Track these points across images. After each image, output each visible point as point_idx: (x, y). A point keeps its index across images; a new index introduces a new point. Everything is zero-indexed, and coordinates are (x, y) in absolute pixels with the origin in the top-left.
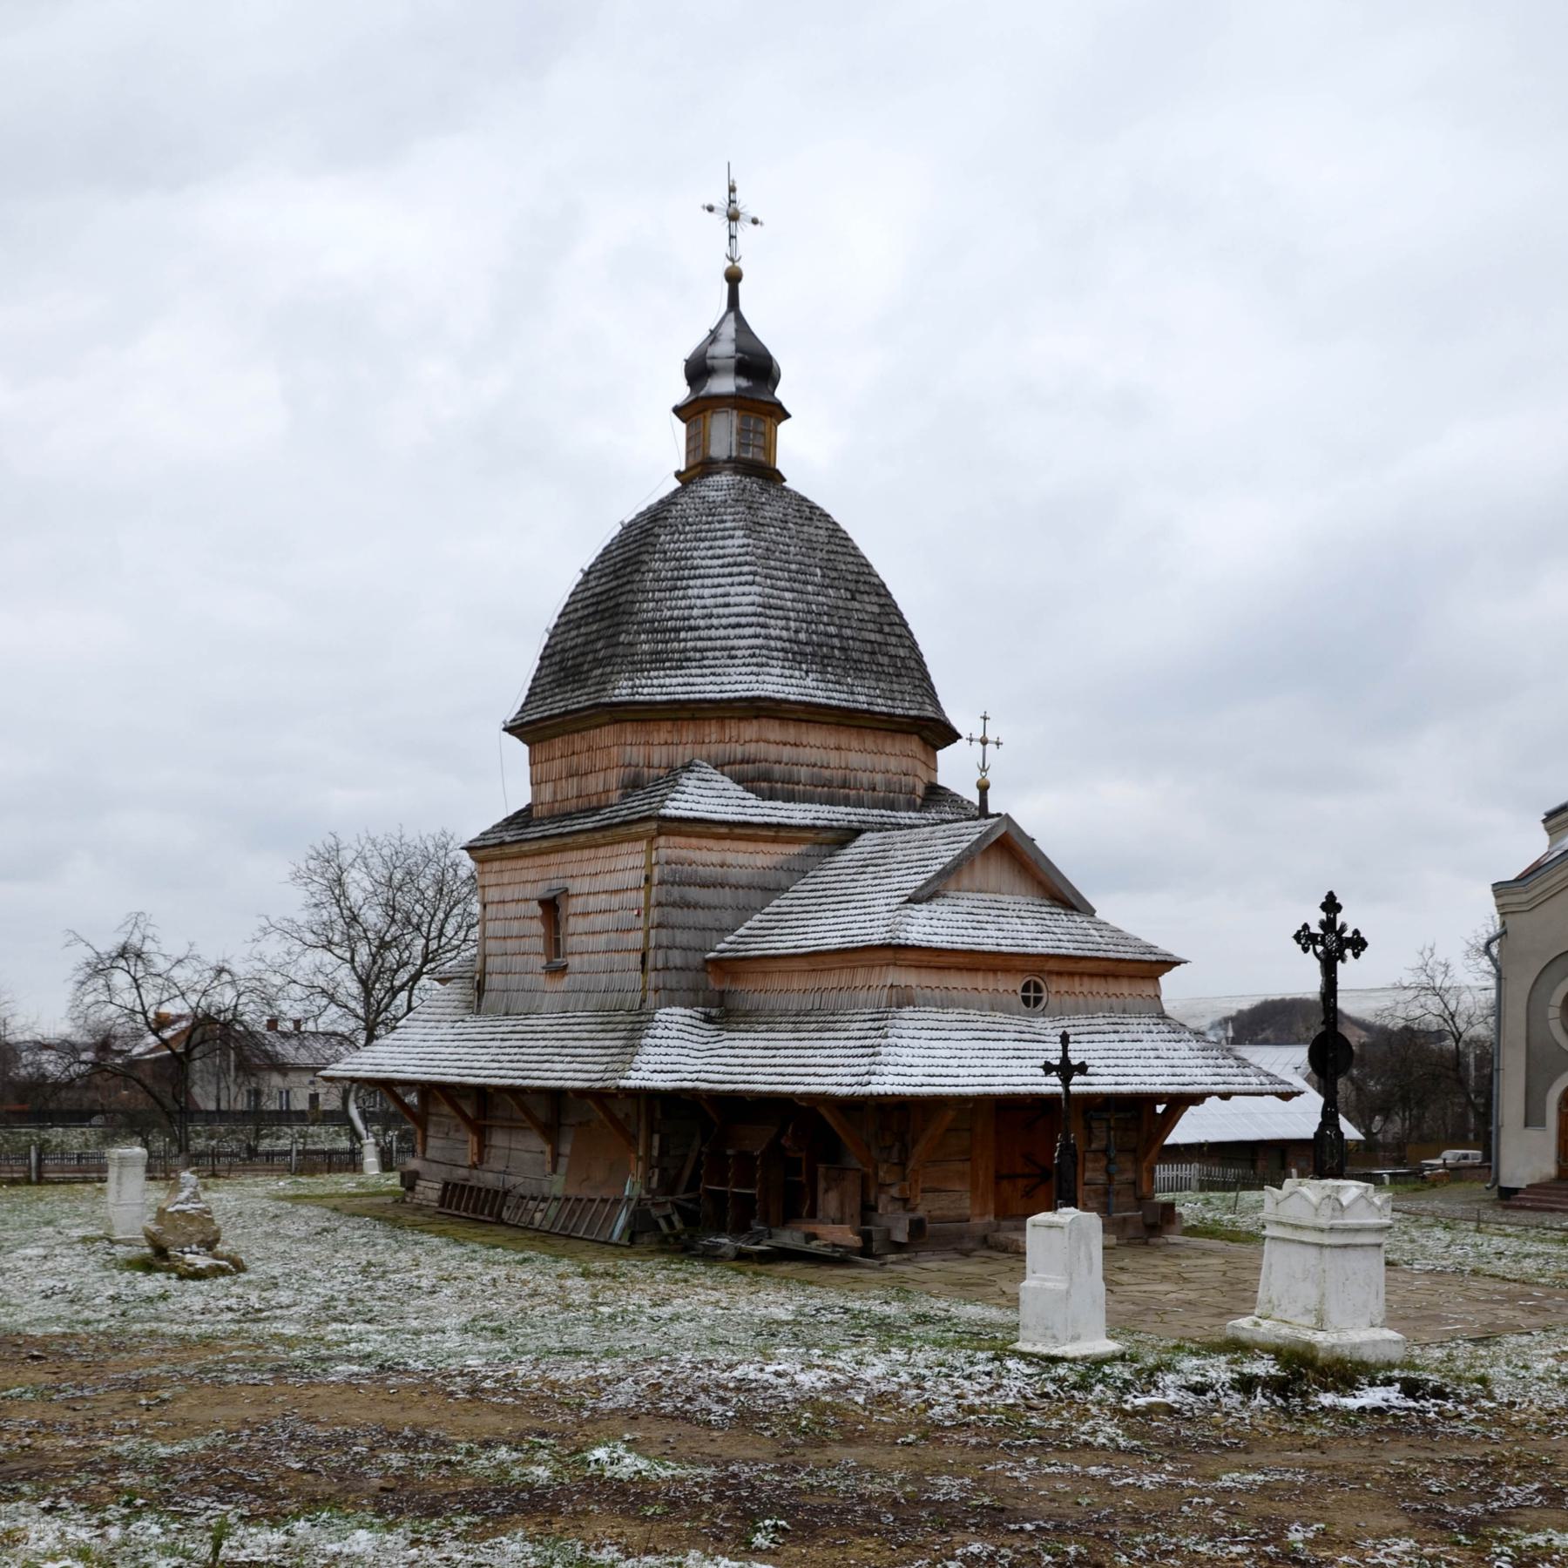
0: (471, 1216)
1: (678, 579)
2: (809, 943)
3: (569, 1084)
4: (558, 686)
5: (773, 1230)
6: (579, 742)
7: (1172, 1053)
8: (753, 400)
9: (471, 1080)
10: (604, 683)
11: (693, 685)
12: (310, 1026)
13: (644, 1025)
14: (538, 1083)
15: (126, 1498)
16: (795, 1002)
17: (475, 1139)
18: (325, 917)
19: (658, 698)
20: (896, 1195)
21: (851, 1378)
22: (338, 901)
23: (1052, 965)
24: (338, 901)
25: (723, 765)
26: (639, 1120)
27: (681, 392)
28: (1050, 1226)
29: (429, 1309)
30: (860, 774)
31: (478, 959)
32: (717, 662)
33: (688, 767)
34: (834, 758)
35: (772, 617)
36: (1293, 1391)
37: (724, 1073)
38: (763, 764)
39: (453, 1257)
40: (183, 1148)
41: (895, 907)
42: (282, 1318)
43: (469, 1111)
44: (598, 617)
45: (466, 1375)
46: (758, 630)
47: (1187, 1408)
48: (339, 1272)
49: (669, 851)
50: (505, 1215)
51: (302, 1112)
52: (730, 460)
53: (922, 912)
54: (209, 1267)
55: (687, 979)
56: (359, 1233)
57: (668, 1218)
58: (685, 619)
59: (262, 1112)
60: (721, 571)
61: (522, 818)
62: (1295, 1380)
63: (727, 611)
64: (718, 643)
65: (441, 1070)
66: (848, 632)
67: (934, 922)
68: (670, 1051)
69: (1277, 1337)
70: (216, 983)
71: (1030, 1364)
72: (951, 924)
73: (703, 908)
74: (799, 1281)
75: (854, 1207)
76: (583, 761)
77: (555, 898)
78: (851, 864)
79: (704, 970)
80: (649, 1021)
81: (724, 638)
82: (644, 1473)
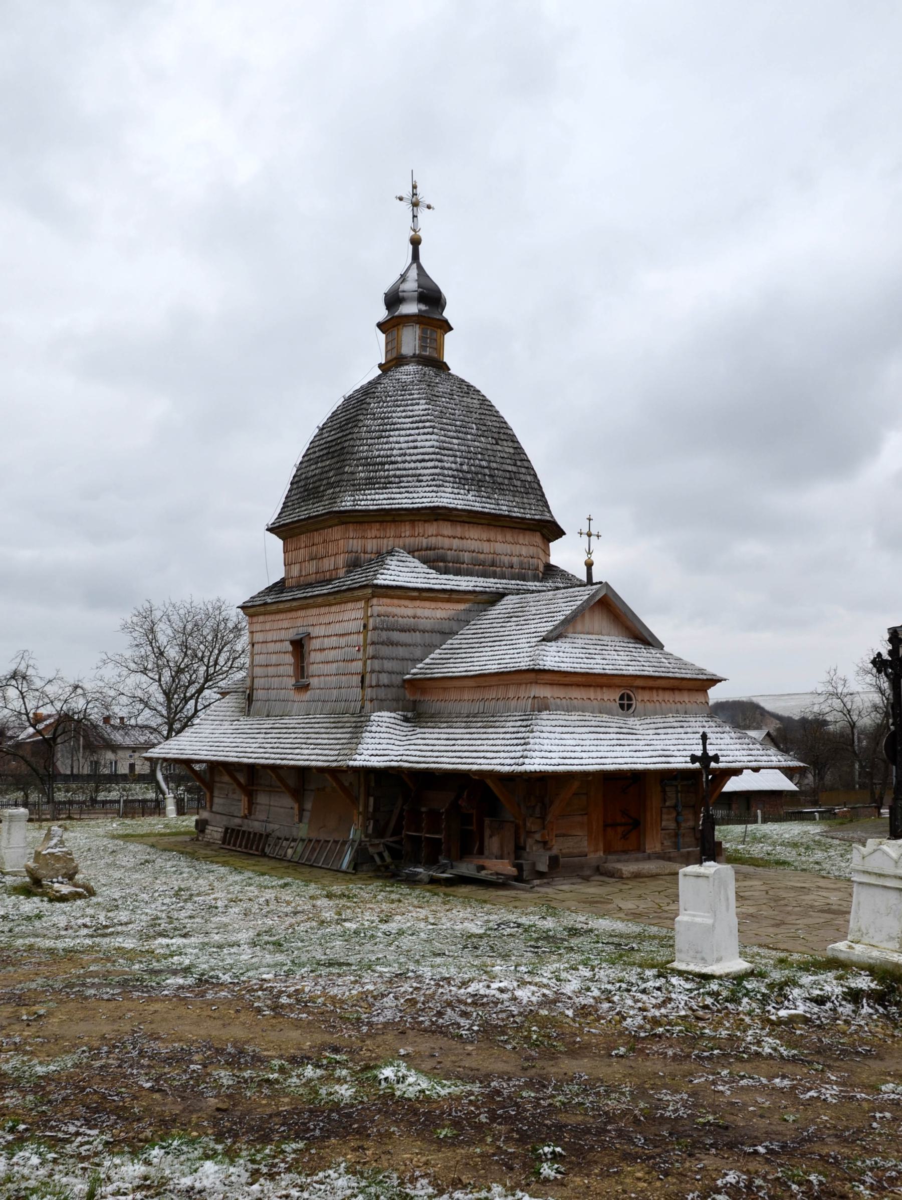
0: (244, 850)
1: (383, 431)
2: (476, 668)
3: (314, 764)
4: (303, 501)
5: (454, 863)
6: (317, 537)
7: (719, 741)
8: (429, 318)
9: (246, 760)
10: (335, 498)
11: (394, 499)
12: (133, 722)
13: (364, 724)
14: (292, 763)
15: (11, 1124)
16: (465, 708)
17: (246, 799)
18: (143, 653)
19: (371, 507)
20: (539, 839)
21: (555, 992)
22: (151, 643)
23: (639, 683)
24: (151, 643)
25: (414, 552)
26: (359, 787)
27: (382, 314)
28: (698, 876)
29: (226, 925)
30: (503, 557)
31: (248, 679)
32: (410, 484)
33: (391, 553)
34: (486, 547)
35: (445, 455)
36: (889, 1001)
37: (419, 756)
39: (236, 882)
40: (50, 801)
41: (534, 644)
42: (122, 933)
43: (242, 780)
44: (330, 456)
45: (265, 990)
46: (437, 463)
47: (815, 1016)
48: (160, 896)
49: (380, 608)
50: (267, 850)
51: (125, 775)
52: (414, 356)
53: (552, 647)
54: (70, 893)
55: (391, 693)
56: (169, 864)
57: (380, 855)
58: (388, 457)
59: (100, 776)
60: (411, 426)
61: (279, 587)
62: (889, 992)
63: (415, 451)
64: (410, 472)
65: (225, 753)
66: (494, 465)
67: (561, 654)
68: (381, 741)
69: (870, 958)
70: (73, 695)
71: (687, 980)
72: (572, 655)
73: (402, 646)
74: (476, 900)
75: (510, 847)
76: (320, 550)
77: (301, 639)
78: (500, 616)
79: (403, 687)
80: (367, 721)
81: (414, 469)
82: (427, 1093)
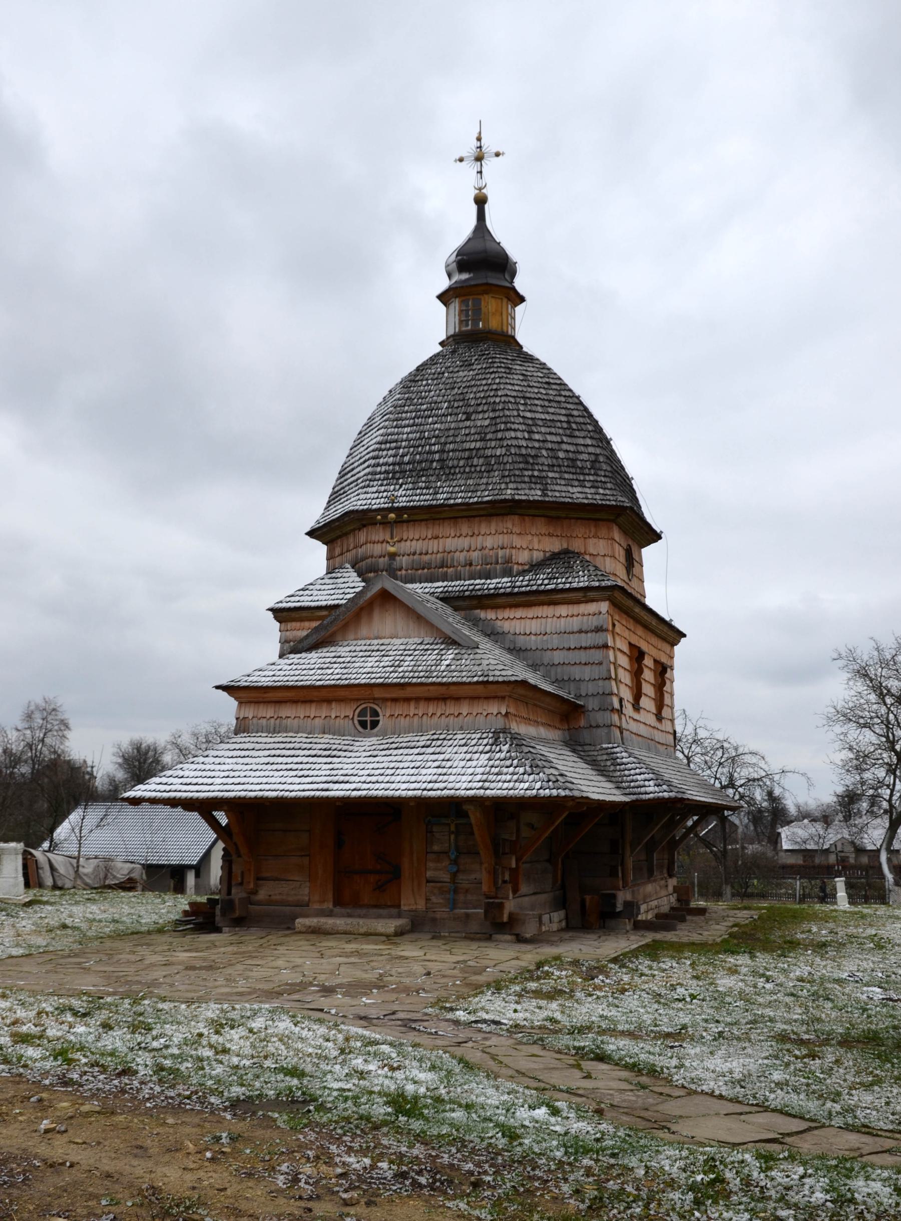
38: (369, 561)
49: (288, 633)
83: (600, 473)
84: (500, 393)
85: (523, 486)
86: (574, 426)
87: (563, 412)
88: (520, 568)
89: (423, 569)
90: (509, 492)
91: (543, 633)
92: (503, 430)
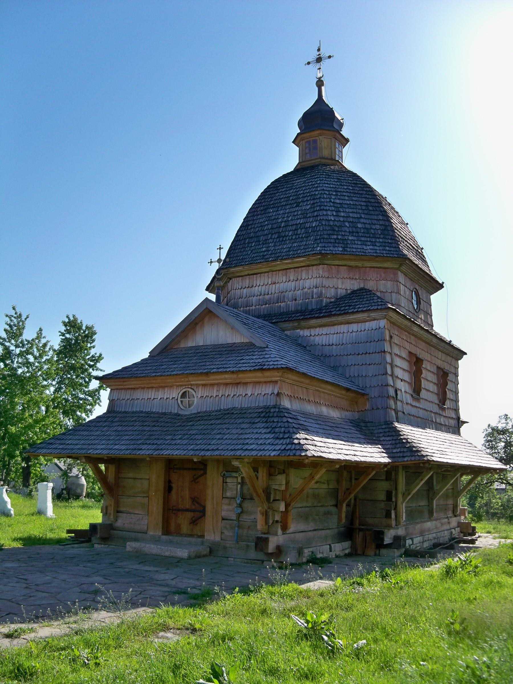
83: (387, 237)
84: (319, 189)
85: (330, 245)
86: (371, 208)
87: (364, 200)
88: (328, 300)
89: (266, 304)
90: (319, 248)
91: (341, 343)
92: (318, 210)
